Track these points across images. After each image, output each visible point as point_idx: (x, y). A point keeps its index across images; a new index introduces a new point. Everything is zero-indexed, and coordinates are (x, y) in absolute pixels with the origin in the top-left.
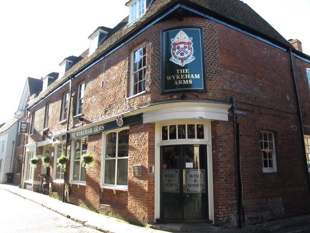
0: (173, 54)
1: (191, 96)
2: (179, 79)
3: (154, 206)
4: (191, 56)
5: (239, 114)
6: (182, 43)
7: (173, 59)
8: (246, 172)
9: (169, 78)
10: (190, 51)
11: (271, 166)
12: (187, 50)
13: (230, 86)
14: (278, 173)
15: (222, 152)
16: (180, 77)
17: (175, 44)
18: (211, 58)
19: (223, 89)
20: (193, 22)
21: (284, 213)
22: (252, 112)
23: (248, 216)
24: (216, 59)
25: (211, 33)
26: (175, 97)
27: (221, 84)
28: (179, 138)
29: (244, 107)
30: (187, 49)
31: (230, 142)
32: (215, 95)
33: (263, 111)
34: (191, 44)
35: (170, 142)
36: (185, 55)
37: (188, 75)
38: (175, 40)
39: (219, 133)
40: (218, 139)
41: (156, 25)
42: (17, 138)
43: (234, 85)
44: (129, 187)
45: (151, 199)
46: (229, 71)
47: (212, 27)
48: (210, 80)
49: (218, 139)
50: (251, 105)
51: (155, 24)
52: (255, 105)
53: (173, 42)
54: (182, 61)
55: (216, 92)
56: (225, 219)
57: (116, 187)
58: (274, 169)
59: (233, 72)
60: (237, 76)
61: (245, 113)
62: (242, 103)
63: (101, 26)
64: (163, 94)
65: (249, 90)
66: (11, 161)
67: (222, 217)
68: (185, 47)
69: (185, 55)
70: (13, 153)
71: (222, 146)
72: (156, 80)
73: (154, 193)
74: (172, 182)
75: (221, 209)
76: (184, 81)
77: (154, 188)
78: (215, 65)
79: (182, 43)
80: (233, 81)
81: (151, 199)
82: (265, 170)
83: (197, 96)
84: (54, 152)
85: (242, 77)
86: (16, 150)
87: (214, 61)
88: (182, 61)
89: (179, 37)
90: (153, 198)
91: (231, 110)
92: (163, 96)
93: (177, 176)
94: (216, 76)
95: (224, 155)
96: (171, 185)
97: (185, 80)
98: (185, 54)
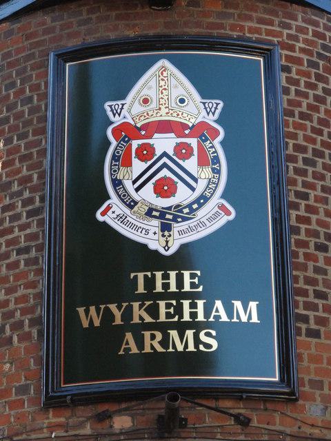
0: (117, 183)
2: (149, 327)
4: (216, 200)
12: (191, 164)
41: (24, 21)
53: (117, 121)
64: (54, 402)
68: (183, 151)
72: (18, 326)
76: (174, 334)
83: (244, 422)
92: (52, 418)
98: (180, 185)
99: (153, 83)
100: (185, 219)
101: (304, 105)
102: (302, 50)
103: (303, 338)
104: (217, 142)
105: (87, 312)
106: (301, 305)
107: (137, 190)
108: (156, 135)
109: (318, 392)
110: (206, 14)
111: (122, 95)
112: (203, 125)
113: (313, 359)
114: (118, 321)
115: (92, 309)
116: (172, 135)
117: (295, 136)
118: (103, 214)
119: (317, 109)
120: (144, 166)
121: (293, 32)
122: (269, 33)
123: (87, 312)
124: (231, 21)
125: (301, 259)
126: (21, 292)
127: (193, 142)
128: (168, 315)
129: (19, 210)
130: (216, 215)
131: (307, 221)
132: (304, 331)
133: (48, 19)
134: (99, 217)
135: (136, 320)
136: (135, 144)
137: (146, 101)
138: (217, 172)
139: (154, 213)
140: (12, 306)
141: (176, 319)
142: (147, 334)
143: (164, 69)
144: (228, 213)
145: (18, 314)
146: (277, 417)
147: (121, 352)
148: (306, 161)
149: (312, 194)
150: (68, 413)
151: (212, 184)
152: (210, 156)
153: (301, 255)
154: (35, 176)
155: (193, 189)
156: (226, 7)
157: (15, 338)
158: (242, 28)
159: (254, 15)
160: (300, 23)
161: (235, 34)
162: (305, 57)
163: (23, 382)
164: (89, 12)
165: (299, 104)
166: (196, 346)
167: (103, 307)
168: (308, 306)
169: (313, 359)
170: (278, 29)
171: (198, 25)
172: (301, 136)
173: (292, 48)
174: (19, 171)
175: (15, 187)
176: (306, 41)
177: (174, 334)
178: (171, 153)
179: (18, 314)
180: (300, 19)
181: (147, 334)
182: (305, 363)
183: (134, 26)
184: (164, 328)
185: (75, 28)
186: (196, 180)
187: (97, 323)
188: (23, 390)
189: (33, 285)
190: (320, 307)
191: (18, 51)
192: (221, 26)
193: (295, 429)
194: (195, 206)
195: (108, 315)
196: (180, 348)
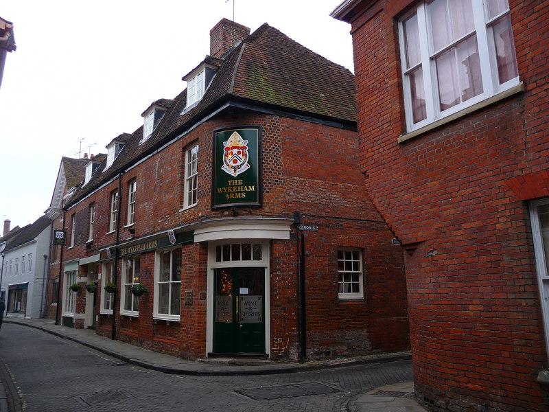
0: (225, 161)
1: (244, 212)
3: (205, 338)
4: (246, 163)
5: (307, 231)
6: (235, 147)
7: (225, 168)
8: (314, 299)
9: (220, 190)
12: (241, 156)
14: (364, 300)
16: (232, 189)
17: (228, 149)
19: (285, 203)
26: (226, 213)
28: (233, 260)
29: (316, 220)
32: (273, 210)
33: (344, 223)
36: (239, 163)
38: (227, 144)
42: (50, 250)
48: (266, 192)
51: (207, 121)
52: (332, 217)
54: (235, 170)
58: (360, 295)
62: (311, 216)
63: (156, 99)
64: (213, 210)
67: (278, 350)
68: (239, 153)
69: (239, 163)
70: (46, 274)
71: (280, 270)
72: (207, 193)
74: (254, 311)
79: (235, 147)
86: (49, 267)
88: (235, 170)
90: (205, 329)
91: (295, 226)
93: (259, 302)
95: (283, 279)
96: (252, 314)
97: (238, 193)
127: (241, 150)
188: (208, 206)
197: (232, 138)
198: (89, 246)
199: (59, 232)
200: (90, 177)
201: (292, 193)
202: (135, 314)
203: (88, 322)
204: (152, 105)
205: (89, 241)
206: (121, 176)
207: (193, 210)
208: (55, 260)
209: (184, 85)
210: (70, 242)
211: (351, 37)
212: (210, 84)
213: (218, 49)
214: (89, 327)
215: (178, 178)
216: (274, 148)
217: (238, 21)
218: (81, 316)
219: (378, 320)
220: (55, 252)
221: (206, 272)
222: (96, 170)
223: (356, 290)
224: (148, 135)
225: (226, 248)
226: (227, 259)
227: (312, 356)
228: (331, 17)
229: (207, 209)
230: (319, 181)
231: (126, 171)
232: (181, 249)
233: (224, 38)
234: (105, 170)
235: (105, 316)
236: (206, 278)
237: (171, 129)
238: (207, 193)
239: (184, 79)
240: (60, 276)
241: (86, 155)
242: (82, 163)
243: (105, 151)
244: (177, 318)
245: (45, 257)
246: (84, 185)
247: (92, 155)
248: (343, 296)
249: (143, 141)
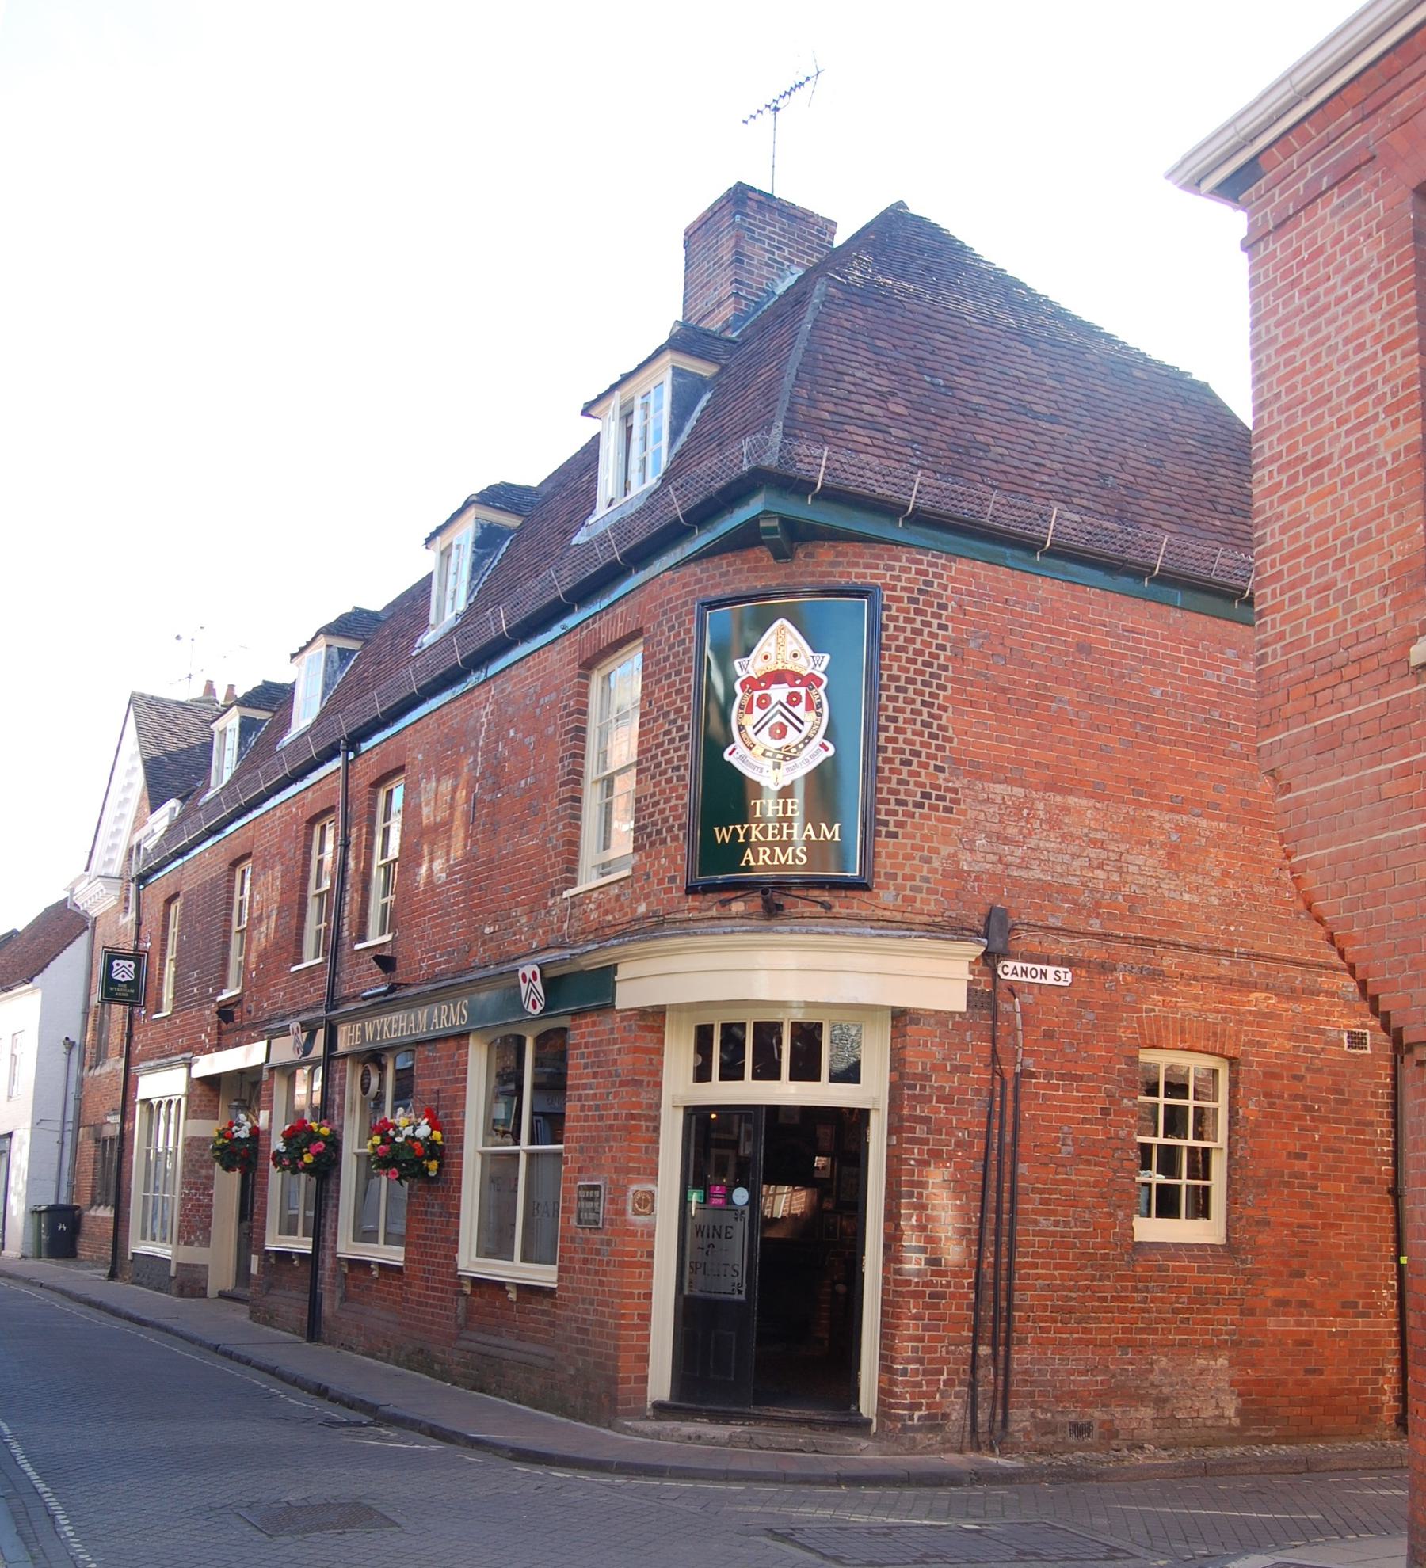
0: (741, 728)
2: (764, 844)
3: (646, 1348)
4: (819, 738)
10: (811, 717)
11: (1201, 1209)
12: (800, 710)
13: (994, 858)
15: (926, 1142)
16: (764, 832)
18: (909, 735)
20: (834, 564)
21: (1236, 1422)
22: (1106, 968)
23: (1033, 1415)
24: (932, 736)
25: (918, 612)
26: (737, 907)
27: (945, 850)
30: (802, 705)
31: (970, 1102)
33: (1168, 962)
34: (819, 682)
35: (721, 1092)
37: (790, 827)
39: (916, 1063)
40: (913, 1087)
41: (682, 570)
43: (1019, 852)
44: (561, 1270)
45: (636, 1321)
46: (999, 788)
47: (928, 583)
48: (890, 835)
49: (913, 1087)
50: (1105, 936)
53: (743, 675)
55: (918, 889)
56: (917, 1414)
57: (515, 1270)
59: (1019, 792)
60: (1040, 806)
61: (1066, 977)
64: (691, 891)
65: (1100, 866)
66: (62, 1143)
68: (794, 699)
71: (926, 1120)
72: (670, 829)
73: (649, 1296)
75: (904, 1372)
76: (778, 850)
77: (651, 1276)
78: (926, 766)
80: (1012, 831)
81: (636, 1321)
82: (1151, 1229)
83: (828, 907)
84: (270, 1108)
85: (1066, 810)
86: (81, 1082)
87: (923, 744)
89: (766, 650)
92: (691, 902)
94: (927, 817)
98: (790, 728)
99: (773, 640)
100: (792, 758)
101: (901, 639)
102: (903, 589)
103: (882, 839)
104: (821, 690)
105: (720, 831)
106: (883, 812)
107: (756, 734)
108: (773, 686)
109: (892, 882)
110: (819, 564)
111: (747, 652)
112: (812, 676)
113: (889, 856)
114: (741, 840)
115: (724, 830)
116: (786, 685)
117: (890, 668)
118: (730, 754)
119: (913, 641)
120: (763, 712)
121: (896, 573)
122: (874, 576)
123: (720, 831)
124: (841, 569)
125: (886, 774)
126: (674, 802)
127: (802, 691)
128: (774, 836)
129: (674, 734)
130: (817, 752)
131: (895, 740)
132: (884, 833)
133: (698, 570)
134: (726, 757)
135: (753, 839)
136: (757, 694)
137: (766, 657)
138: (820, 715)
139: (768, 754)
140: (667, 813)
141: (778, 838)
142: (761, 850)
143: (783, 627)
144: (826, 749)
145: (671, 819)
146: (855, 902)
147: (743, 864)
148: (898, 689)
149: (901, 717)
150: (701, 898)
151: (816, 726)
152: (816, 701)
153: (887, 769)
154: (685, 708)
155: (800, 731)
156: (837, 556)
157: (669, 839)
158: (849, 575)
159: (861, 561)
160: (904, 564)
161: (843, 580)
162: (905, 595)
163: (673, 874)
164: (729, 565)
165: (896, 638)
166: (794, 861)
167: (731, 827)
168: (888, 812)
169: (889, 856)
170: (883, 572)
171: (812, 574)
172: (895, 668)
173: (894, 588)
174: (674, 703)
175: (672, 716)
176: (908, 580)
177: (778, 850)
178: (784, 701)
179: (671, 819)
180: (904, 560)
181: (761, 850)
182: (883, 859)
183: (762, 577)
184: (771, 845)
185: (717, 580)
186: (802, 723)
187: (727, 840)
188: (672, 879)
189: (680, 797)
190: (900, 812)
191: (678, 598)
192: (831, 574)
193: (870, 912)
194: (801, 746)
195: (735, 833)
196: (783, 861)
197: (768, 643)
198: (225, 1013)
199: (122, 962)
200: (315, 710)
201: (981, 841)
202: (395, 1255)
203: (221, 1276)
204: (467, 504)
205: (226, 995)
206: (347, 762)
207: (615, 890)
208: (100, 1057)
209: (591, 427)
210: (160, 995)
211: (1243, 261)
212: (688, 429)
213: (713, 297)
214: (222, 1295)
215: (561, 773)
216: (922, 673)
217: (788, 191)
218: (194, 1255)
219: (1271, 1323)
220: (99, 1029)
221: (656, 1119)
222: (252, 740)
223: (1201, 1209)
224: (450, 618)
225: (732, 1035)
226: (732, 1071)
227: (1027, 1434)
228: (1169, 183)
229: (668, 891)
230: (1084, 802)
231: (365, 746)
232: (563, 1031)
233: (739, 259)
234: (287, 739)
235: (284, 1256)
236: (656, 1141)
237: (533, 595)
238: (670, 829)
239: (586, 412)
240: (126, 1112)
241: (210, 688)
242: (206, 709)
243: (282, 674)
244: (544, 1275)
245: (70, 1044)
246: (209, 795)
247: (231, 687)
248: (1151, 1229)
249: (428, 638)
